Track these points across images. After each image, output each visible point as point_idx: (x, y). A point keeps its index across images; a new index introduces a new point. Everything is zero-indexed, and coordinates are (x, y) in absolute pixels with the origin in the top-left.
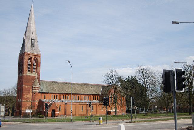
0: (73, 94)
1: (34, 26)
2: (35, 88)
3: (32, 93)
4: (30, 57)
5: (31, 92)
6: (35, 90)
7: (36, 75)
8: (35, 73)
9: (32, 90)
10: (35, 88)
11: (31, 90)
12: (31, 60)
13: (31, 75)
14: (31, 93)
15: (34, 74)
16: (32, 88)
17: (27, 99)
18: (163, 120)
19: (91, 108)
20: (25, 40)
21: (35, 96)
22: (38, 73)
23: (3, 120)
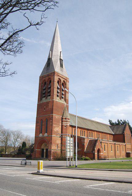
0: (78, 127)
1: (60, 41)
2: (65, 119)
3: (62, 126)
4: (59, 79)
5: (60, 124)
6: (67, 121)
7: (65, 103)
8: (63, 100)
9: (62, 121)
10: (65, 119)
11: (61, 121)
12: (60, 83)
13: (60, 101)
14: (61, 126)
15: (62, 101)
16: (62, 119)
17: (57, 133)
18: (97, 163)
19: (104, 149)
20: (52, 59)
21: (66, 129)
22: (66, 100)
23: (68, 165)
